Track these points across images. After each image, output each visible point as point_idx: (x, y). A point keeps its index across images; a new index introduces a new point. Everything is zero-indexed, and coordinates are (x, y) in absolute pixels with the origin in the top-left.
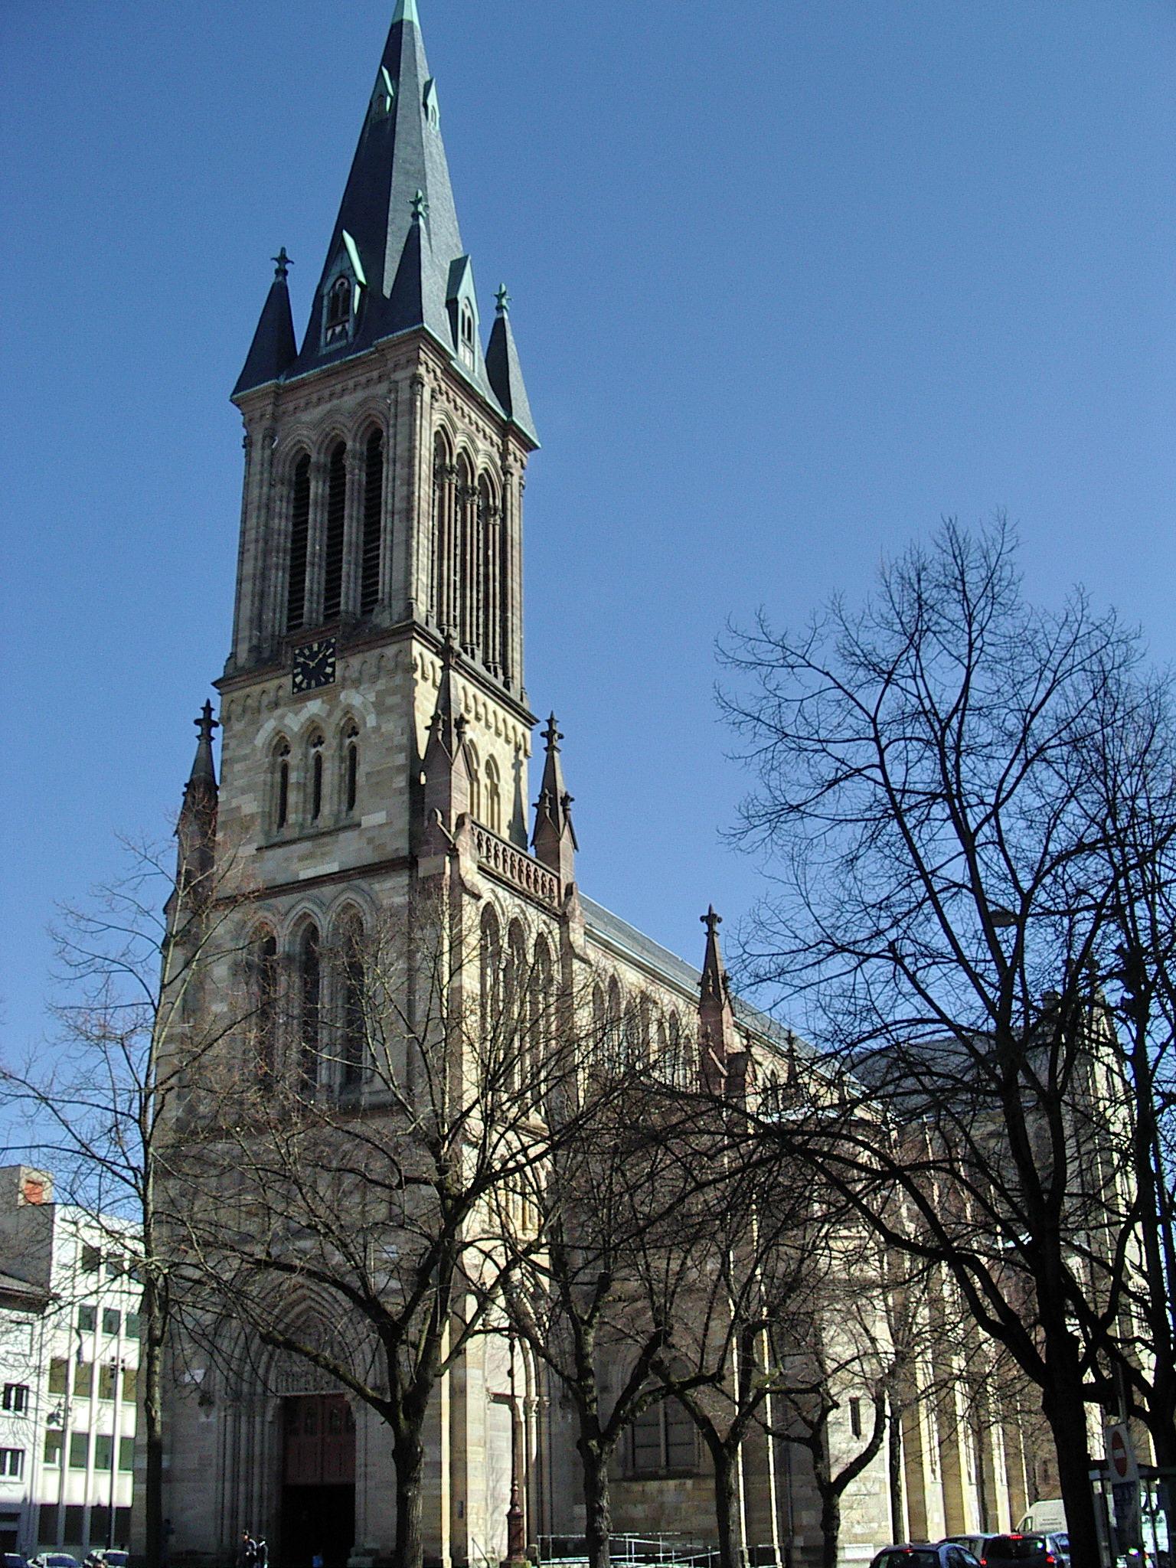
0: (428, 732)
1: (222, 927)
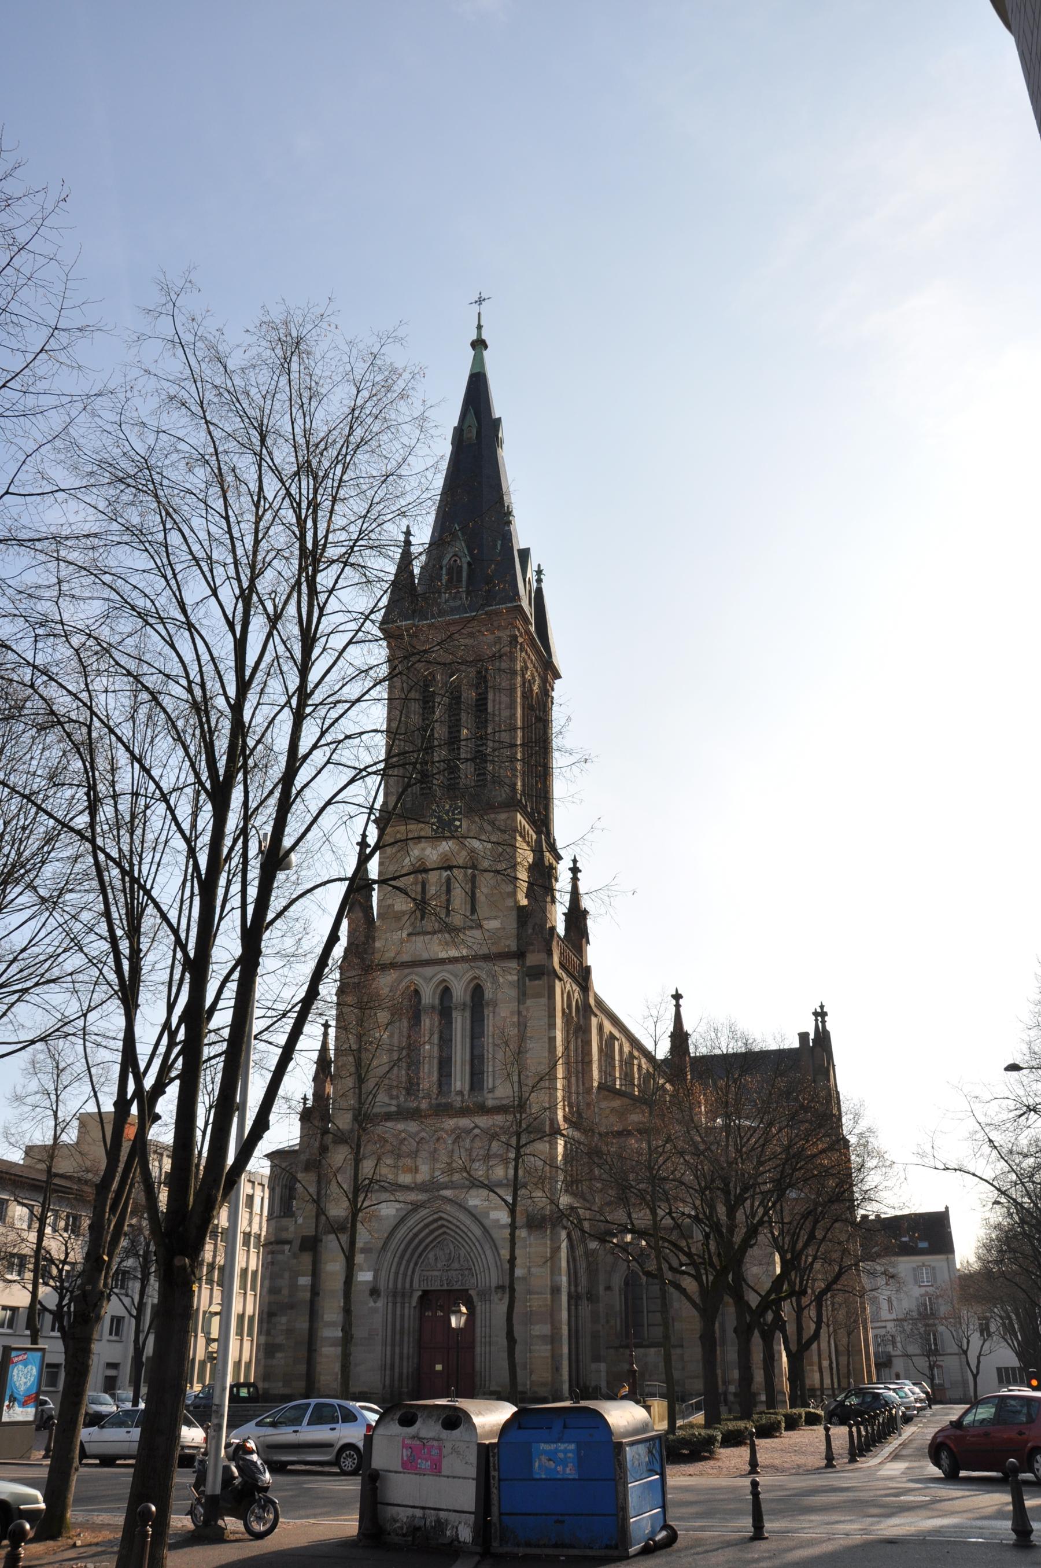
0: (796, 1044)
1: (385, 982)
